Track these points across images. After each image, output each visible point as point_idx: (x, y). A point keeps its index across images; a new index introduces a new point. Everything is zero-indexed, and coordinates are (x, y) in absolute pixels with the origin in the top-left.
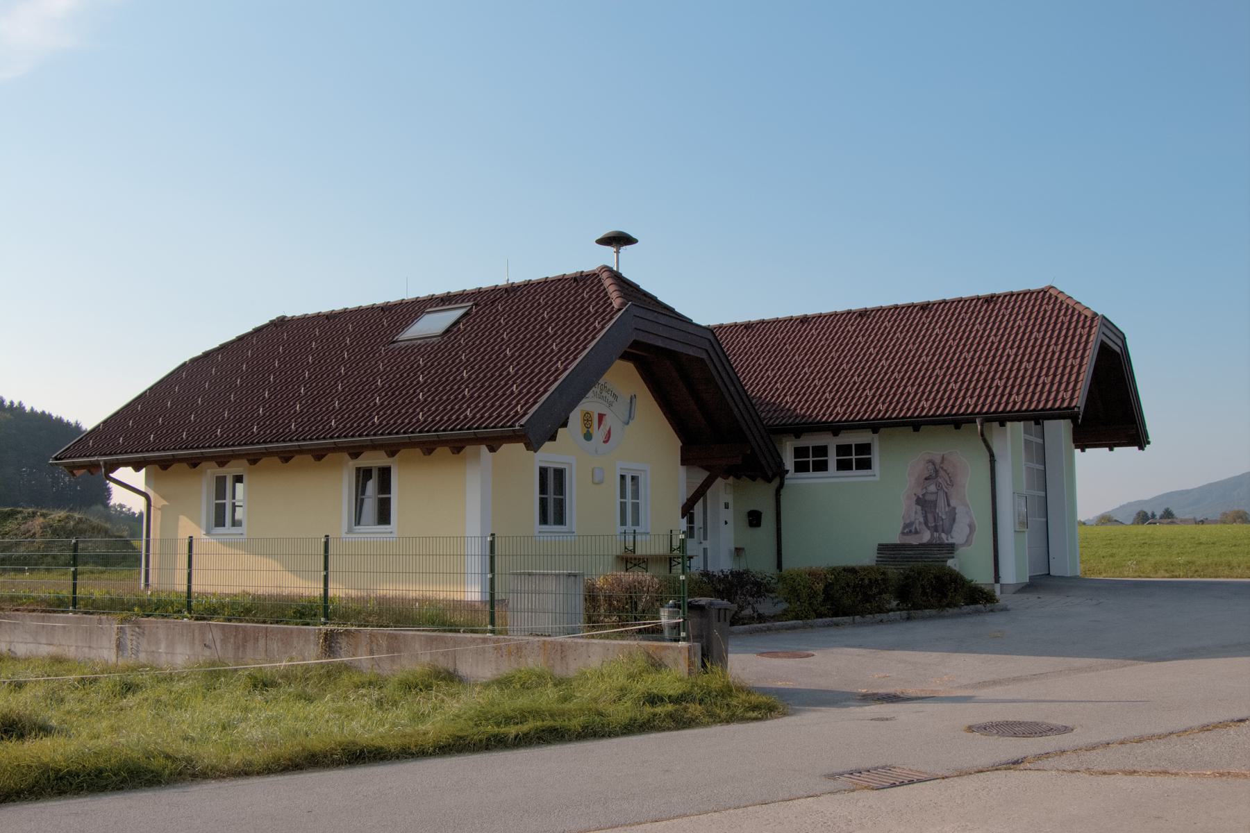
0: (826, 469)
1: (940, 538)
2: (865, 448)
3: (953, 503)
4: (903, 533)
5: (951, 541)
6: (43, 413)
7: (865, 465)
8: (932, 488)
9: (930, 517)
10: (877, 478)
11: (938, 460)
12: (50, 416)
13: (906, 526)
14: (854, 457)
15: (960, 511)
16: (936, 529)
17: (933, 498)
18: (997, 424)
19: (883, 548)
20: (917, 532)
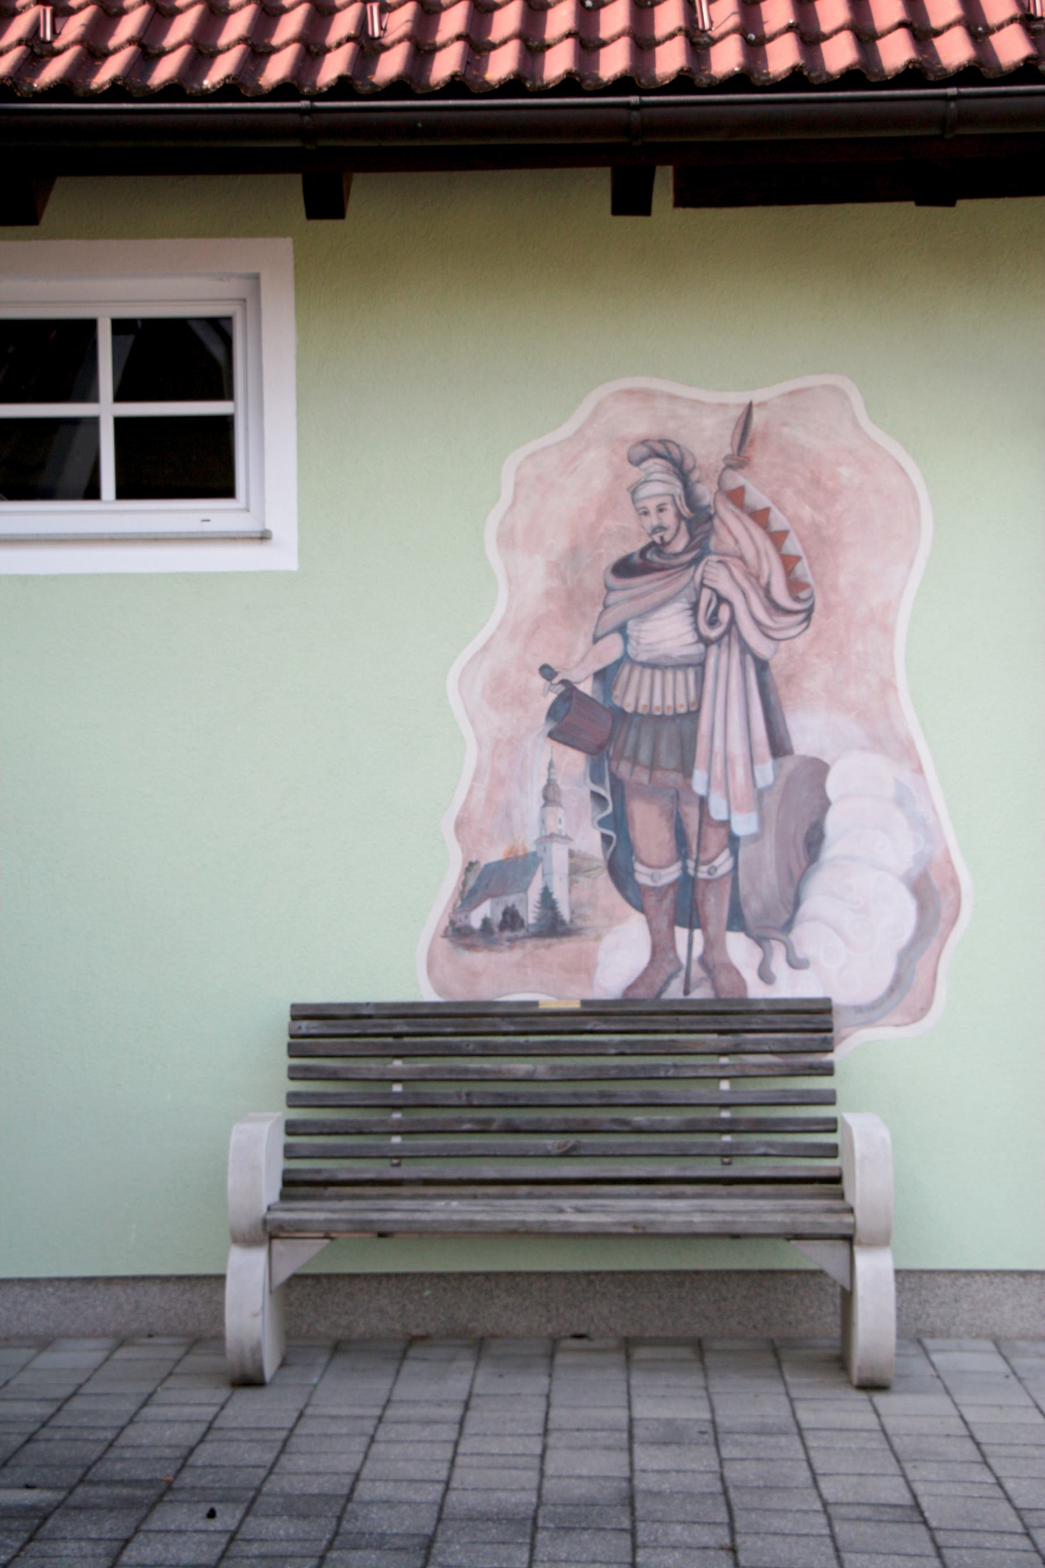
0: (222, 486)
1: (712, 963)
2: (185, 355)
3: (806, 733)
4: (458, 933)
5: (791, 986)
6: (951, 203)
7: (188, 463)
8: (669, 631)
9: (649, 825)
10: (281, 557)
11: (707, 441)
12: (919, 203)
13: (480, 882)
14: (106, 410)
15: (856, 787)
16: (686, 905)
17: (667, 694)
18: (598, 183)
19: (325, 1035)
20: (553, 926)
